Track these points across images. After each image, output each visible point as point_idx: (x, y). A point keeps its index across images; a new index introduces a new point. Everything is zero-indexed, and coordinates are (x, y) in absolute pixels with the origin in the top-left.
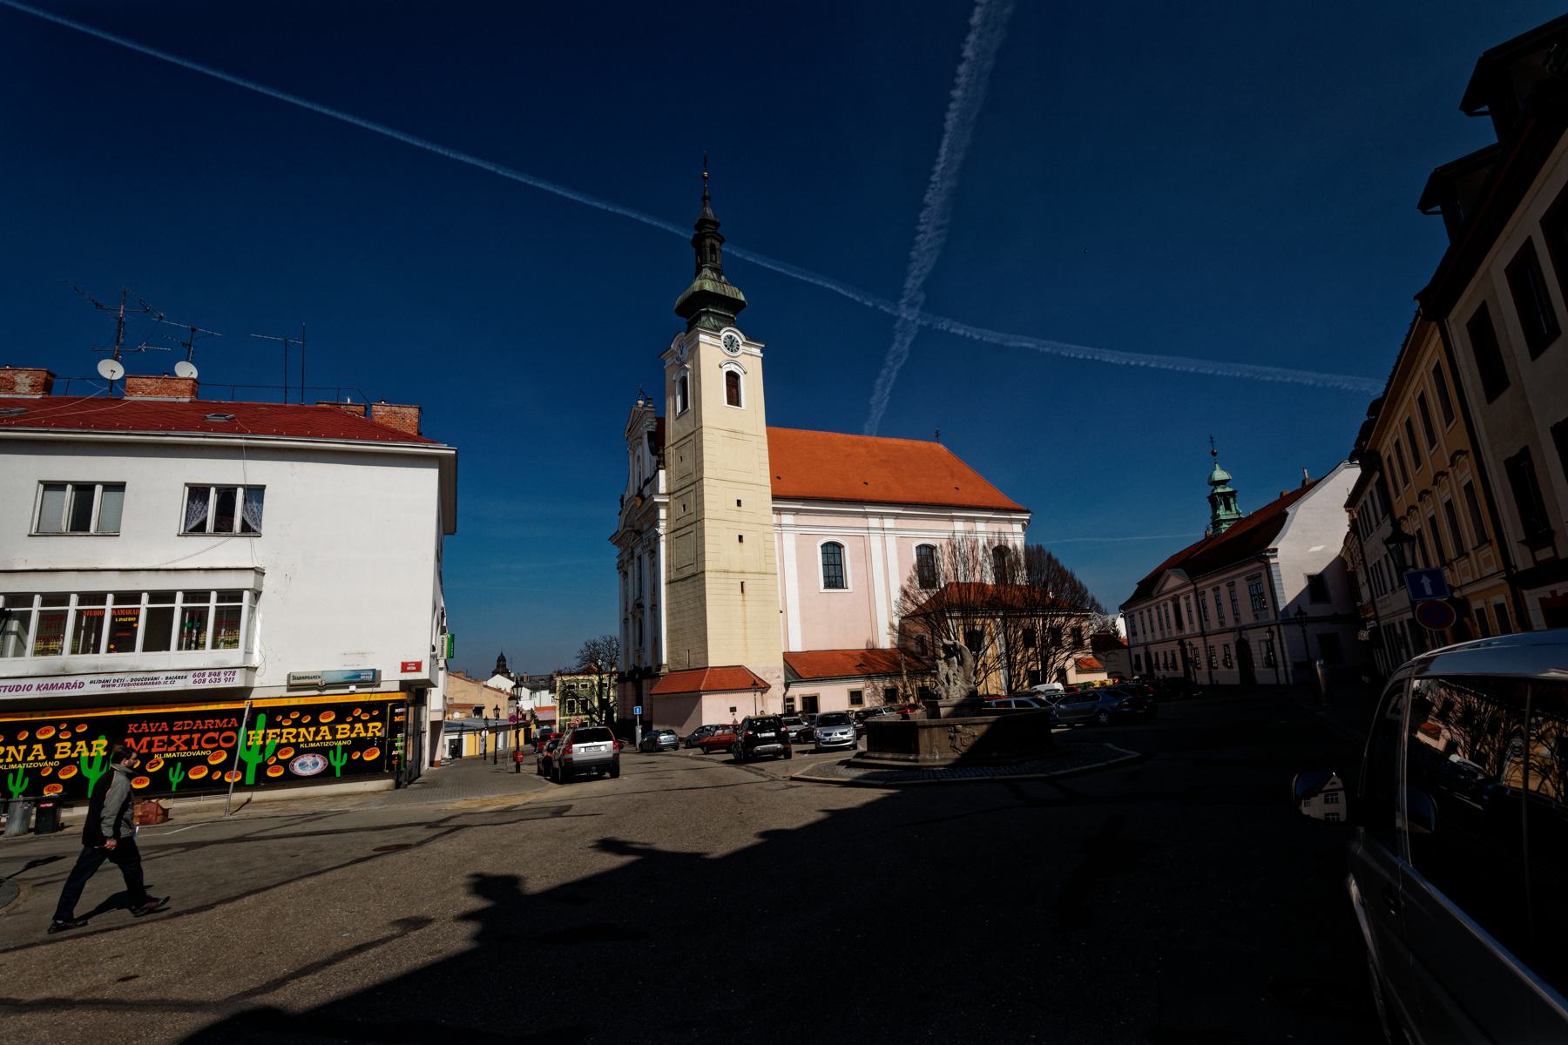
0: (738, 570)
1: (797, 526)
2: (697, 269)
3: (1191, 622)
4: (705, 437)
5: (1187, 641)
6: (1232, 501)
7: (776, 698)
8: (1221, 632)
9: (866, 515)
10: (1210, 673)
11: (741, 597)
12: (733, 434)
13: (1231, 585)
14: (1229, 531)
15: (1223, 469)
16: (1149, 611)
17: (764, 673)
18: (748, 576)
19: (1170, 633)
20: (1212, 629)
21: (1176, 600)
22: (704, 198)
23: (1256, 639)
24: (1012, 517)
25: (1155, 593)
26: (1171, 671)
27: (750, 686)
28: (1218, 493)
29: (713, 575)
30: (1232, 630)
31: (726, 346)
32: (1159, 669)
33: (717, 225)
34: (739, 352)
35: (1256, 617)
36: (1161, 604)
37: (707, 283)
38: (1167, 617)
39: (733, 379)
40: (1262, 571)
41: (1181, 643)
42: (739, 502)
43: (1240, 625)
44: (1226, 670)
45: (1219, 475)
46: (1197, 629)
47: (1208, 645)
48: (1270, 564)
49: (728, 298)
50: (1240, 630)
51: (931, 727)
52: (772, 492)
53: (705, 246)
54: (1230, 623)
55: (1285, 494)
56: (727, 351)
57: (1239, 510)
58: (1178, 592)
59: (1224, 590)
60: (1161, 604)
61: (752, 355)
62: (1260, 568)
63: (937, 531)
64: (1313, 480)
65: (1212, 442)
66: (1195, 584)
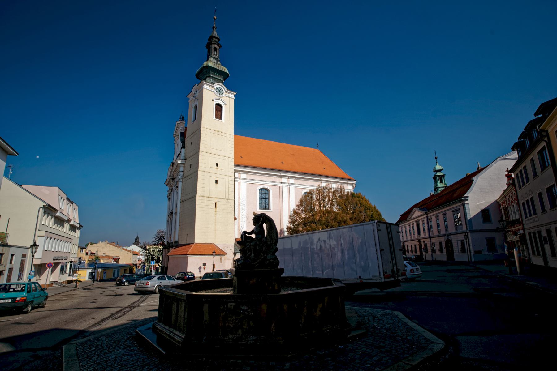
0: (214, 197)
1: (248, 179)
2: (208, 58)
3: (424, 232)
4: (202, 132)
5: (422, 241)
6: (443, 179)
7: (229, 259)
8: (438, 236)
9: (281, 176)
10: (432, 255)
11: (214, 210)
12: (217, 132)
13: (445, 215)
14: (442, 192)
15: (440, 165)
16: (405, 227)
17: (224, 248)
18: (220, 200)
19: (414, 237)
20: (434, 235)
21: (418, 222)
22: (213, 28)
23: (456, 241)
24: (348, 182)
25: (408, 219)
26: (414, 254)
27: (212, 253)
28: (437, 175)
29: (201, 198)
30: (444, 235)
31: (217, 92)
32: (408, 252)
33: (219, 39)
34: (223, 95)
35: (456, 229)
36: (411, 224)
37: (211, 63)
38: (413, 230)
39: (219, 108)
40: (460, 208)
41: (419, 241)
42: (217, 165)
43: (448, 233)
44: (440, 253)
45: (438, 167)
46: (427, 235)
47: (432, 242)
48: (464, 204)
49: (220, 70)
50: (448, 235)
51: (458, 249)
52: (234, 162)
53: (211, 48)
54: (443, 232)
55: (468, 175)
56: (217, 94)
57: (449, 182)
58: (418, 219)
59: (441, 216)
60: (411, 224)
61: (229, 97)
62: (460, 206)
63: (311, 185)
64: (482, 167)
65: (435, 153)
66: (427, 214)
